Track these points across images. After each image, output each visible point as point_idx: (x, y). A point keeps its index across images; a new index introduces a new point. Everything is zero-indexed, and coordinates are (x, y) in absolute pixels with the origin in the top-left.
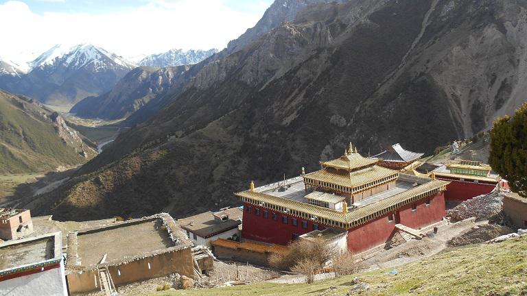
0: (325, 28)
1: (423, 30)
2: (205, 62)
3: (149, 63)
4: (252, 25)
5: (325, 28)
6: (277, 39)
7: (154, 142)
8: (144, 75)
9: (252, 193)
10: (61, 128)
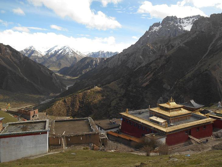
5: (164, 47)
6: (143, 50)
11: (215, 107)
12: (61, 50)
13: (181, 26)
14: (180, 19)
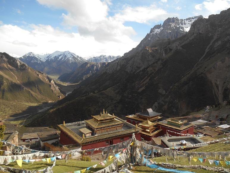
0: (162, 50)
1: (205, 53)
2: (117, 59)
3: (92, 61)
4: (135, 47)
5: (162, 50)
6: (142, 54)
7: (85, 94)
8: (89, 65)
9: (63, 126)
10: (52, 85)
11: (202, 112)
12: (61, 55)
13: (182, 28)
14: (182, 20)
